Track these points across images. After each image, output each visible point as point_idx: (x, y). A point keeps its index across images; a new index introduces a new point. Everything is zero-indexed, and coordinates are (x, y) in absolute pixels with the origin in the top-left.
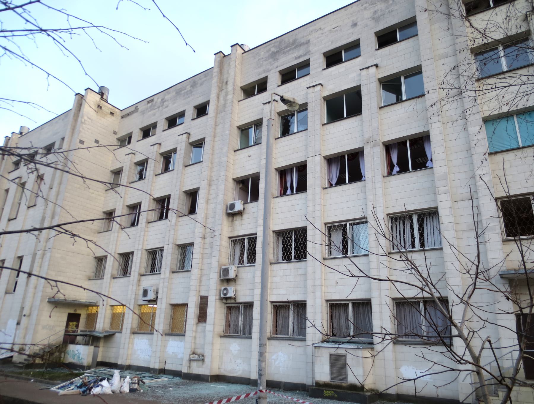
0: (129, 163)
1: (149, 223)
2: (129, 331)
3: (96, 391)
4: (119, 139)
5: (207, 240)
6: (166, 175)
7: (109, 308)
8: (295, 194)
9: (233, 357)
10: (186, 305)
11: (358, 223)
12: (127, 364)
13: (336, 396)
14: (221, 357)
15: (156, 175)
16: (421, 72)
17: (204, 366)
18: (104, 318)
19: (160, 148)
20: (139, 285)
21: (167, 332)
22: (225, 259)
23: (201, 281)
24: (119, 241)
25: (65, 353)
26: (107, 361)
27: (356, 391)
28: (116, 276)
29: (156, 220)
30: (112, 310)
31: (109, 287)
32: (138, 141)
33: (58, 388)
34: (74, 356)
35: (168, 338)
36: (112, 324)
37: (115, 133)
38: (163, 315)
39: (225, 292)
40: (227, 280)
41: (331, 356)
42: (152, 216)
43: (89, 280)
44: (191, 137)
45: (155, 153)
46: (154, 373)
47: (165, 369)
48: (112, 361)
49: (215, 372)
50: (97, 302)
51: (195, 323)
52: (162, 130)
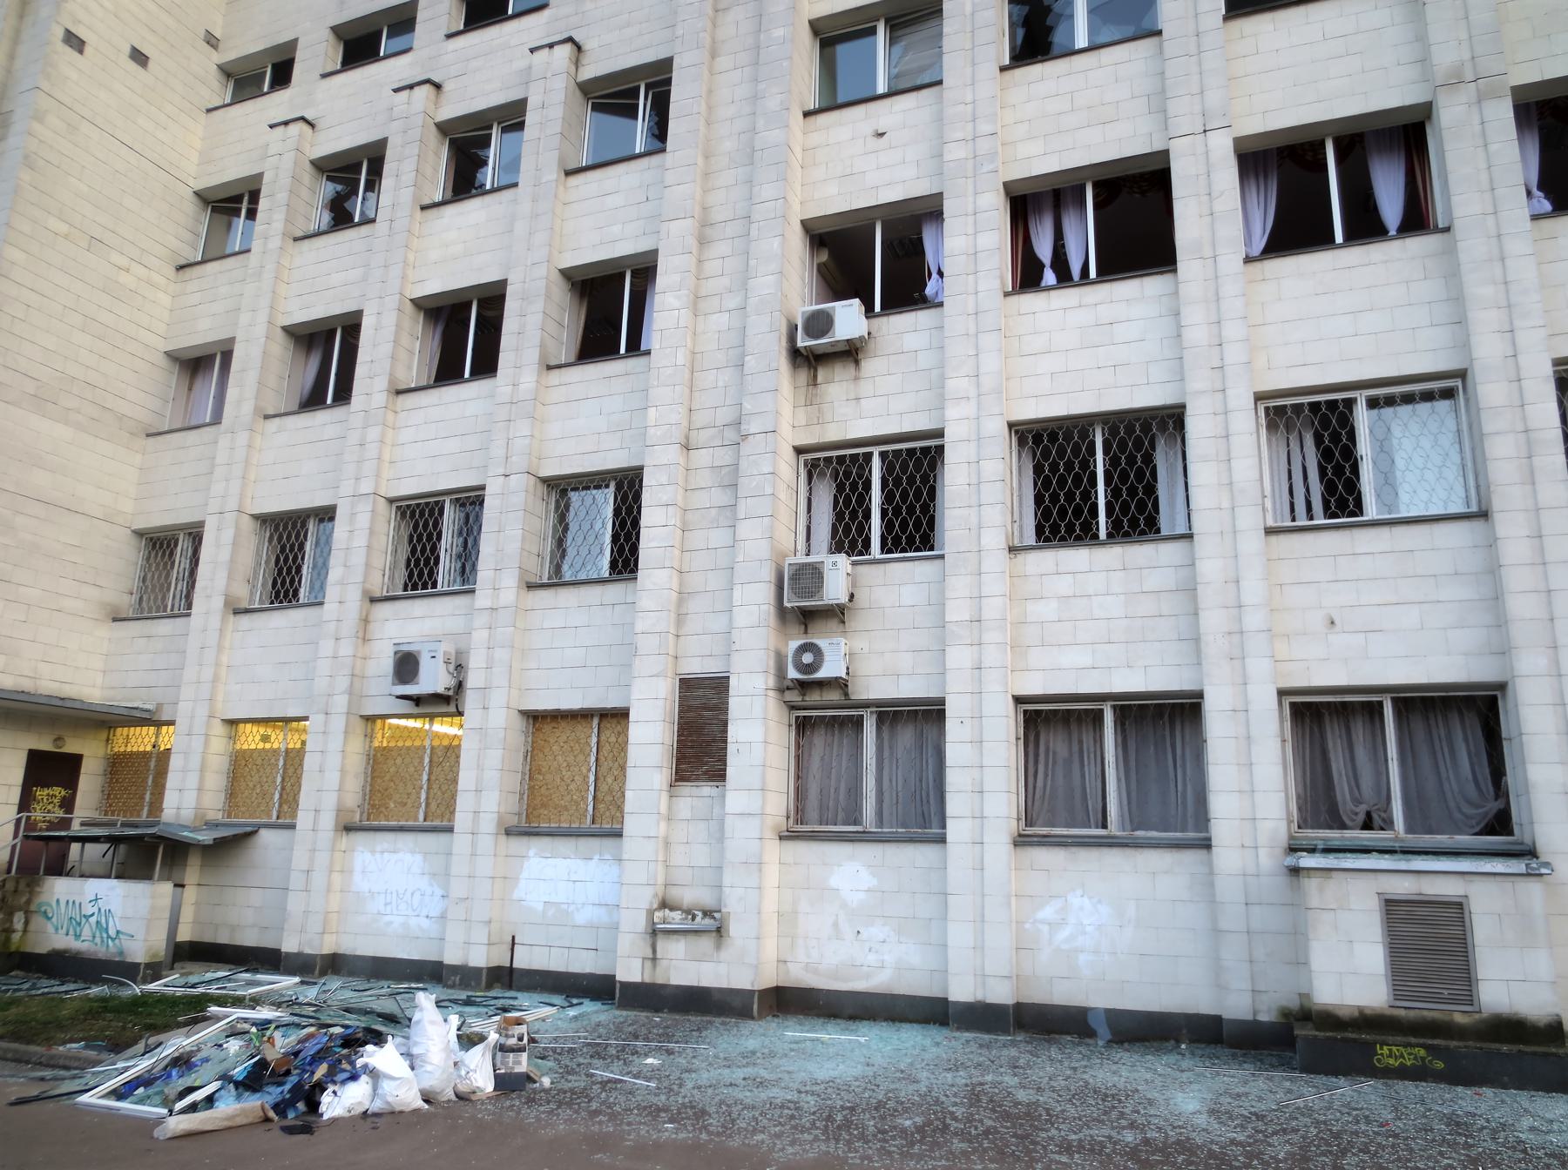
0: (289, 158)
1: (399, 392)
2: (328, 820)
3: (340, 1102)
4: (227, 71)
5: (702, 458)
6: (472, 210)
7: (219, 729)
8: (1094, 283)
9: (837, 914)
10: (620, 715)
11: (1408, 399)
12: (326, 951)
13: (1440, 1065)
14: (788, 919)
15: (423, 208)
16: (332, 519)
17: (725, 954)
18: (202, 770)
19: (437, 104)
20: (364, 631)
21: (514, 821)
22: (788, 536)
23: (680, 619)
24: (271, 457)
25: (28, 914)
26: (223, 938)
27: (1526, 1042)
28: (245, 605)
29: (424, 383)
30: (233, 738)
31: (220, 648)
32: (324, 76)
33: (118, 1094)
34: (76, 923)
35: (517, 844)
36: (232, 793)
37: (212, 41)
38: (495, 757)
39: (807, 658)
40: (805, 611)
41: (1391, 906)
42: (410, 368)
43: (115, 620)
44: (585, 60)
45: (419, 120)
46: (464, 985)
47: (511, 970)
48: (249, 938)
49: (768, 978)
50: (159, 706)
51: (665, 786)
52: (445, 32)
